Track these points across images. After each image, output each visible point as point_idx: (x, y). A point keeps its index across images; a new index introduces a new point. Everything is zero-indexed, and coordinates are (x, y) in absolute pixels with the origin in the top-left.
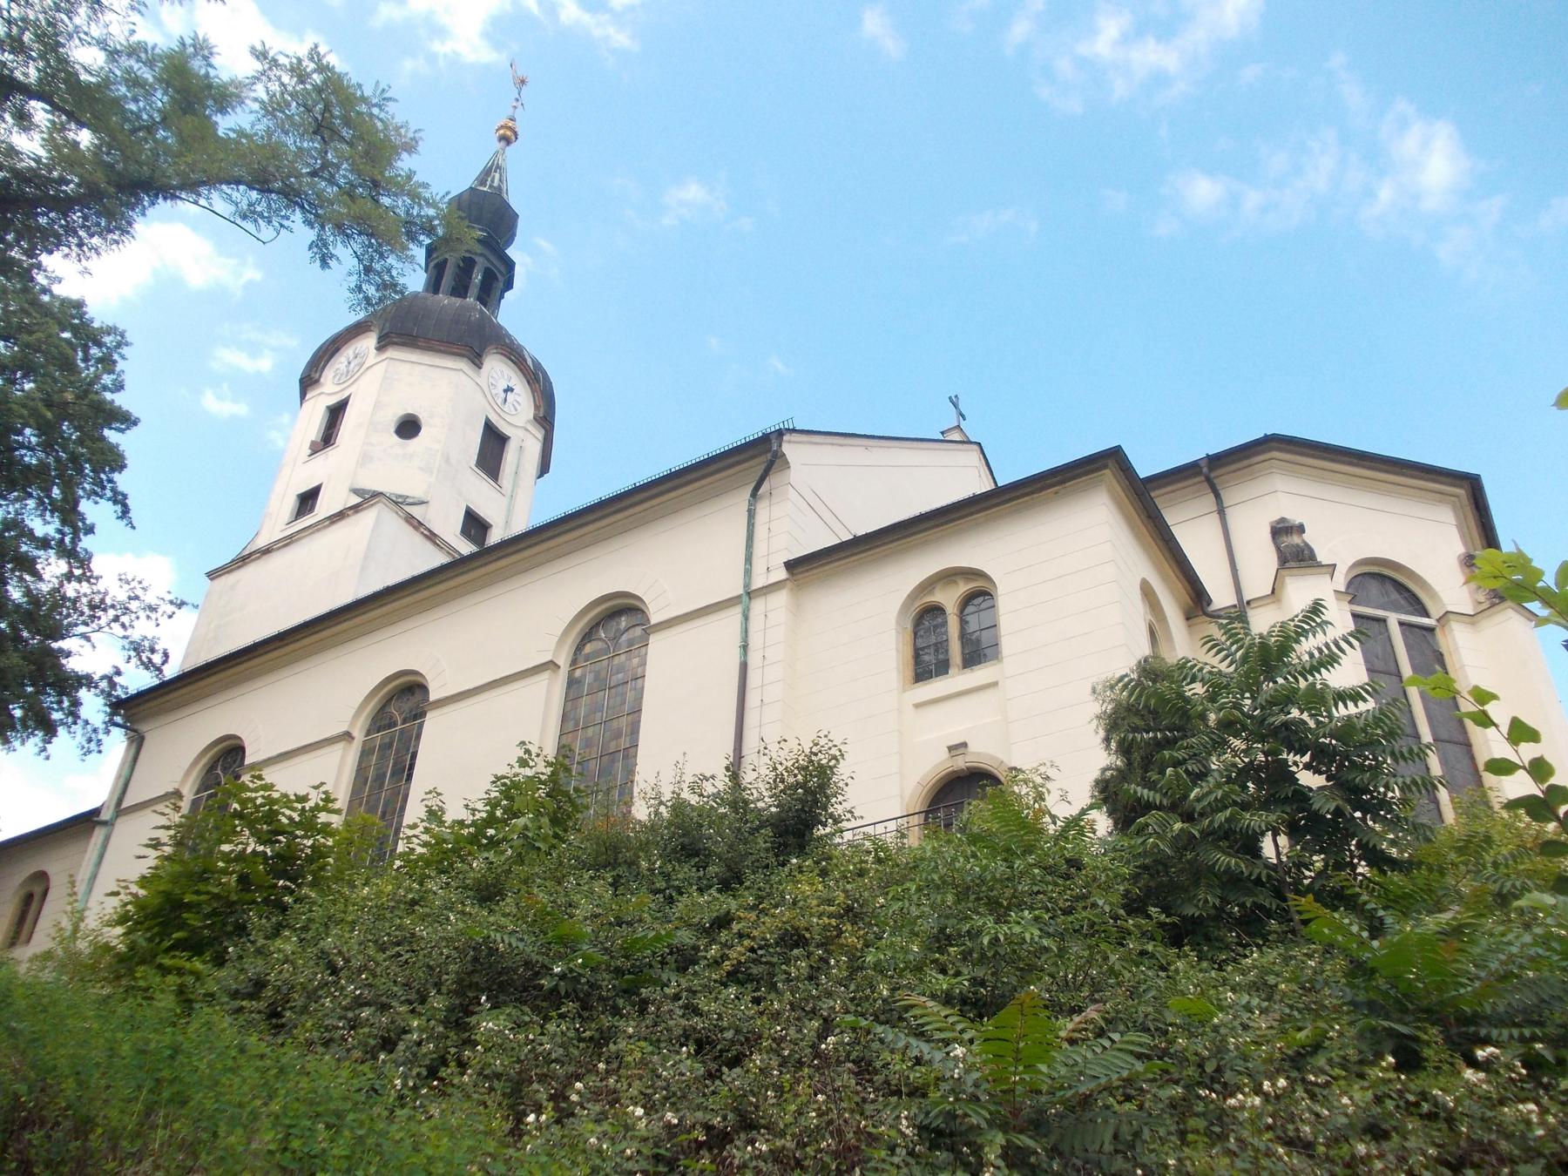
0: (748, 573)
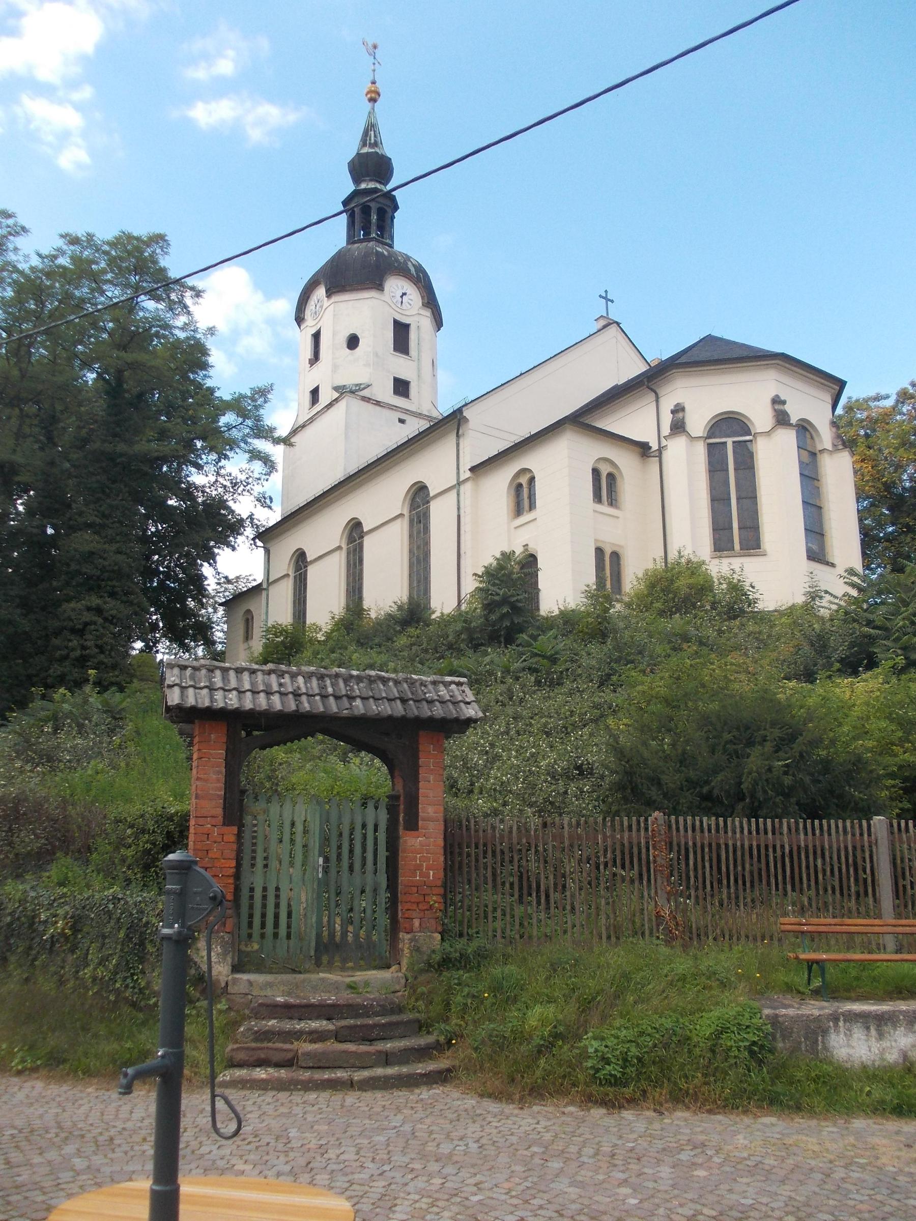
0: (458, 473)
